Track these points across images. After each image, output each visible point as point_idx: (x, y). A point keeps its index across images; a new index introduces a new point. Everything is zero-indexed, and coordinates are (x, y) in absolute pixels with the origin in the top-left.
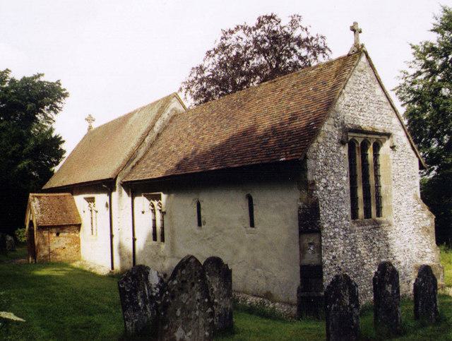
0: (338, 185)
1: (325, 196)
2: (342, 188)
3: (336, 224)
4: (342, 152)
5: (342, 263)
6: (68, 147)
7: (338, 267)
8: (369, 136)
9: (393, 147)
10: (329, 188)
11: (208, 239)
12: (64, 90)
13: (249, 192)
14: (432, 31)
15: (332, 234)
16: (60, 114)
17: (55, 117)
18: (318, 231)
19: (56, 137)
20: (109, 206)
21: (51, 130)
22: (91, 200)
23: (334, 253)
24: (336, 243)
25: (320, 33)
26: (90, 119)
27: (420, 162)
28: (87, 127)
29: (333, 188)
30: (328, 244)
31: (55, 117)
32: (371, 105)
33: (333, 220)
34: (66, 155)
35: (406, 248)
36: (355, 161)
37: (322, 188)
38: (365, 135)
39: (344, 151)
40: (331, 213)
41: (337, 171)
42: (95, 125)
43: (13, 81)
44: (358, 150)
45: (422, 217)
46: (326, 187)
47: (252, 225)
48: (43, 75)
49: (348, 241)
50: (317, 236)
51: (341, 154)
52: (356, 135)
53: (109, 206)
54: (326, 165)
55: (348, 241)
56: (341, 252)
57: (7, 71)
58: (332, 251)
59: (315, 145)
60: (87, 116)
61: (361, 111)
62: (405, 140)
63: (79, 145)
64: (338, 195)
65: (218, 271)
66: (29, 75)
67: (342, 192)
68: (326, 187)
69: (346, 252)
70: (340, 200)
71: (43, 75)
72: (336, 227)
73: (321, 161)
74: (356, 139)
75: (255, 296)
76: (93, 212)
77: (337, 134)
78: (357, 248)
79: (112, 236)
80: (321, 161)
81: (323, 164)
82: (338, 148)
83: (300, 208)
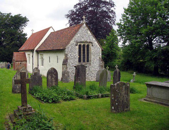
6: (28, 36)
9: (21, 63)
12: (27, 19)
13: (57, 55)
14: (124, 8)
17: (24, 28)
18: (66, 65)
21: (22, 31)
22: (29, 54)
23: (72, 70)
26: (32, 30)
27: (102, 49)
28: (32, 33)
31: (24, 28)
33: (72, 62)
34: (27, 39)
37: (69, 55)
39: (77, 47)
42: (34, 32)
43: (12, 16)
46: (71, 55)
48: (21, 15)
57: (10, 13)
59: (68, 46)
62: (97, 44)
66: (16, 14)
67: (75, 56)
68: (71, 55)
71: (21, 15)
75: (126, 81)
77: (75, 43)
79: (33, 64)
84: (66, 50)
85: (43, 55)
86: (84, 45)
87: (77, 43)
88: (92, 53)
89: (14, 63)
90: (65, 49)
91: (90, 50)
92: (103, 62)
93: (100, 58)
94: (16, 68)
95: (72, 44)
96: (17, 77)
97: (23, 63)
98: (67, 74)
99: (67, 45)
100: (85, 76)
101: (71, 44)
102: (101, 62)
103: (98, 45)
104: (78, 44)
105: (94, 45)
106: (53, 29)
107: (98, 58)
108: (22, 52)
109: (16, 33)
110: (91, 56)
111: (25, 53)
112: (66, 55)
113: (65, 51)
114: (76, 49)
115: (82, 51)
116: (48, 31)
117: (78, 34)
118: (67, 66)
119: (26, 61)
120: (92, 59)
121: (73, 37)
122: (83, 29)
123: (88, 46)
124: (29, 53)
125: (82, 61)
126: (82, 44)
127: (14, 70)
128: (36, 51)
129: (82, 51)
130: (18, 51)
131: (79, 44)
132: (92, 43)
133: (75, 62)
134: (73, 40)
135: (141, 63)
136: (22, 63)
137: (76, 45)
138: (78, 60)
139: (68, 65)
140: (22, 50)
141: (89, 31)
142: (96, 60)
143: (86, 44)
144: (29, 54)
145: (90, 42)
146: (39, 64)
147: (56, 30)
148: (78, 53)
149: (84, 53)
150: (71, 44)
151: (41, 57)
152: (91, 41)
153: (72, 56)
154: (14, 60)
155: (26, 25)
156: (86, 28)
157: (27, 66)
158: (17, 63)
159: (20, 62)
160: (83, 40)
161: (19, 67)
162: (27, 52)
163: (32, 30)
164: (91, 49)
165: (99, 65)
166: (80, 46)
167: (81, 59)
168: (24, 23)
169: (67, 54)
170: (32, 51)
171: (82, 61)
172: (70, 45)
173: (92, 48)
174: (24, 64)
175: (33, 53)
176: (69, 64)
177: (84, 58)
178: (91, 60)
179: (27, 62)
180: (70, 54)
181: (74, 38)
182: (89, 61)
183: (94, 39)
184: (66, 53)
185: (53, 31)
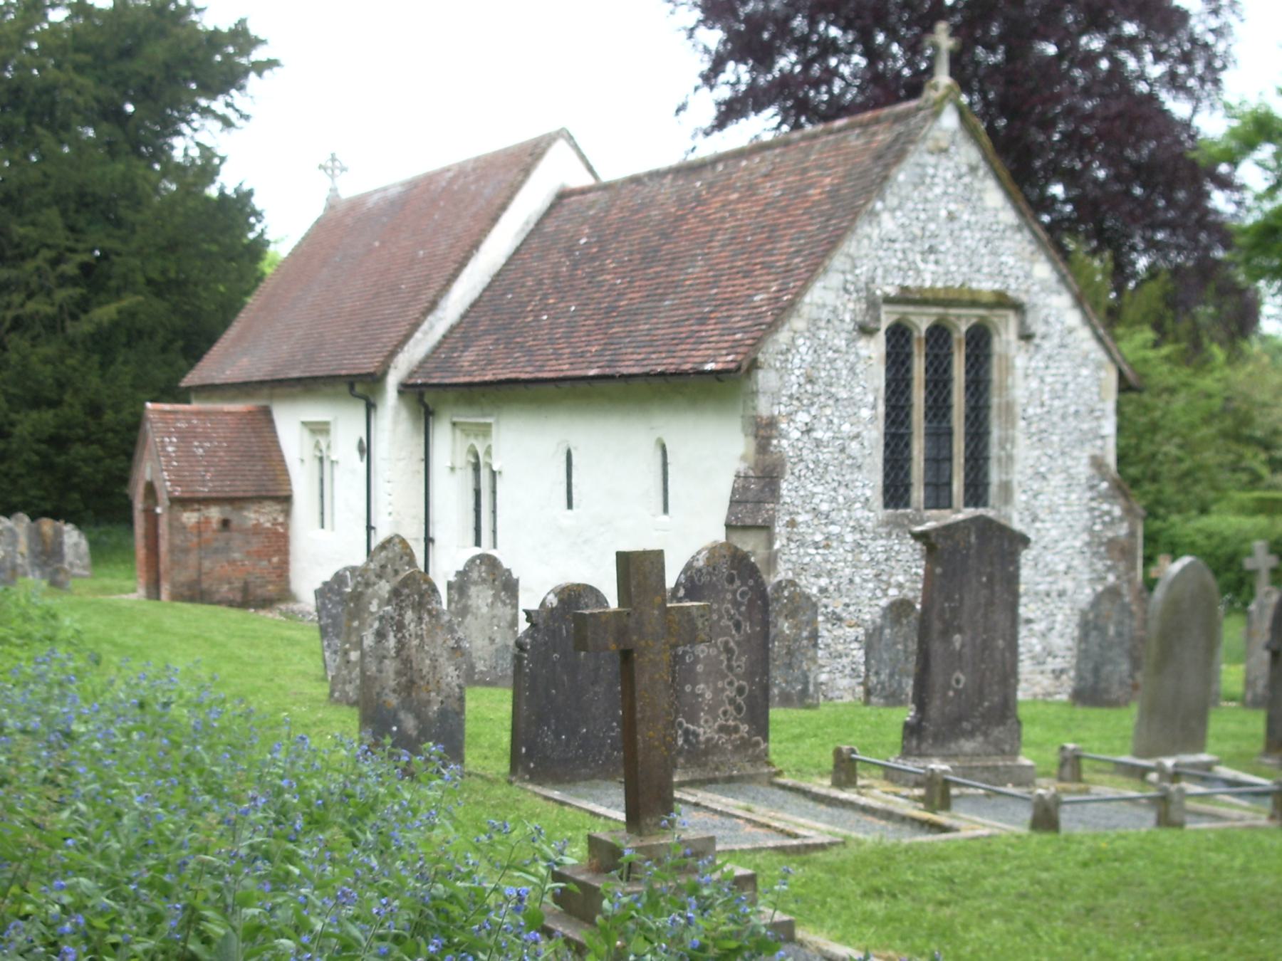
0: (846, 427)
1: (805, 452)
2: (857, 436)
3: (833, 514)
4: (864, 352)
5: (847, 605)
7: (834, 613)
8: (953, 311)
9: (225, 523)
10: (818, 434)
11: (585, 542)
15: (818, 537)
16: (241, 129)
19: (236, 191)
20: (365, 450)
22: (319, 429)
23: (823, 582)
24: (832, 559)
25: (710, 138)
26: (332, 166)
29: (830, 434)
30: (807, 560)
32: (967, 233)
35: (1055, 587)
36: (948, 369)
37: (796, 434)
38: (939, 310)
39: (875, 349)
40: (819, 489)
41: (843, 394)
42: (349, 189)
44: (920, 345)
45: (1108, 513)
46: (808, 430)
47: (666, 510)
49: (865, 557)
50: (762, 535)
51: (857, 355)
52: (910, 309)
53: (365, 450)
54: (810, 381)
55: (865, 557)
56: (845, 581)
58: (817, 576)
59: (783, 337)
60: (325, 159)
61: (932, 250)
62: (1073, 318)
63: (304, 239)
64: (842, 450)
65: (490, 578)
67: (854, 446)
68: (808, 430)
69: (857, 580)
70: (849, 462)
72: (833, 523)
73: (797, 372)
74: (913, 319)
76: (327, 464)
77: (851, 309)
78: (891, 575)
80: (797, 372)
81: (802, 380)
82: (850, 342)
83: (738, 476)
84: (766, 379)
85: (485, 430)
86: (939, 335)
87: (873, 304)
88: (1018, 410)
89: (152, 519)
90: (754, 365)
91: (1004, 388)
92: (1128, 511)
93: (1097, 463)
94: (184, 576)
95: (825, 314)
96: (400, 626)
97: (255, 516)
98: (792, 614)
99: (773, 327)
100: (1013, 606)
101: (814, 322)
102: (1117, 511)
103: (1084, 333)
104: (886, 321)
105: (1038, 328)
106: (582, 157)
107: (1083, 470)
108: (233, 399)
109: (137, 202)
110: (1007, 440)
111: (266, 416)
112: (763, 432)
113: (755, 393)
114: (860, 368)
115: (918, 396)
116: (527, 171)
117: (885, 217)
118: (770, 542)
119: (285, 500)
120: (1016, 478)
121: (833, 243)
122: (931, 160)
123: (980, 340)
124: (316, 412)
125: (918, 494)
126: (922, 322)
127: (154, 591)
128: (405, 389)
129: (918, 396)
130: (182, 396)
131: (887, 318)
132: (1018, 308)
133: (849, 503)
134: (834, 279)
135: (1217, 263)
136: (235, 519)
137: (865, 330)
138: (878, 478)
139: (780, 529)
140: (219, 379)
141: (991, 184)
142: (1057, 480)
143: (962, 322)
144: (319, 429)
145: (1003, 302)
146: (435, 532)
147: (606, 176)
148: (881, 409)
149: (938, 407)
150: (814, 322)
151: (463, 459)
152: (1014, 289)
153: (818, 443)
154: (151, 490)
155: (246, 117)
156: (968, 154)
157: (292, 558)
158: (190, 517)
159: (215, 513)
160: (929, 276)
161: (207, 564)
162: (292, 397)
163: (332, 166)
164: (1009, 368)
165: (1090, 531)
166: (899, 337)
167: (908, 474)
168: (224, 90)
169: (772, 423)
170: (359, 389)
171: (918, 494)
172: (798, 324)
173: (1020, 361)
174: (257, 530)
175: (370, 407)
176: (792, 524)
177: (938, 460)
178: (1006, 488)
179: (287, 513)
180: (803, 417)
181: (838, 261)
182: (993, 490)
183: (1043, 270)
184: (764, 407)
185: (581, 179)
